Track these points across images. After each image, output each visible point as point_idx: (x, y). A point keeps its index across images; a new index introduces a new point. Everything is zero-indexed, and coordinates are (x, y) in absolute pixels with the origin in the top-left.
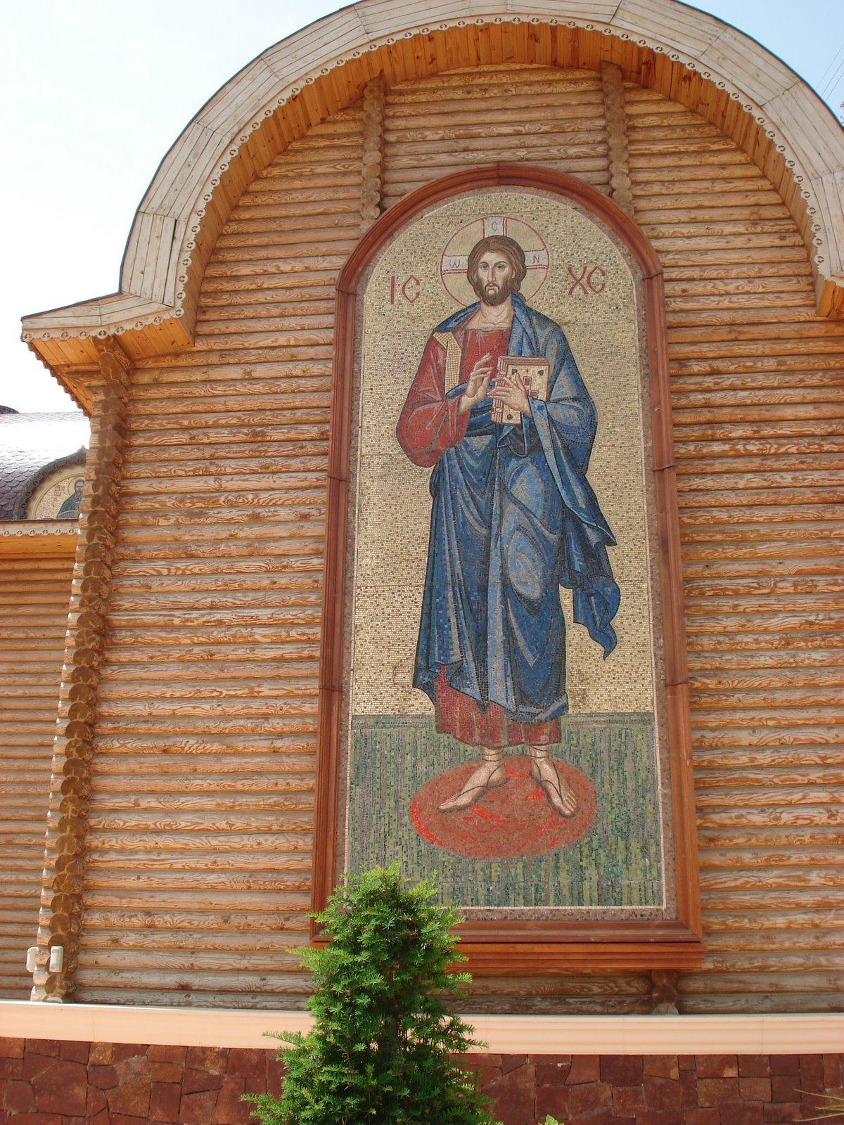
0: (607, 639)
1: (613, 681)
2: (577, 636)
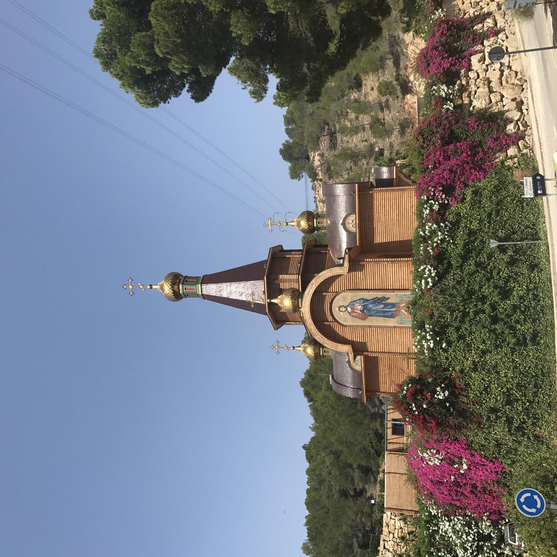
0: (388, 298)
1: (393, 298)
2: (388, 301)
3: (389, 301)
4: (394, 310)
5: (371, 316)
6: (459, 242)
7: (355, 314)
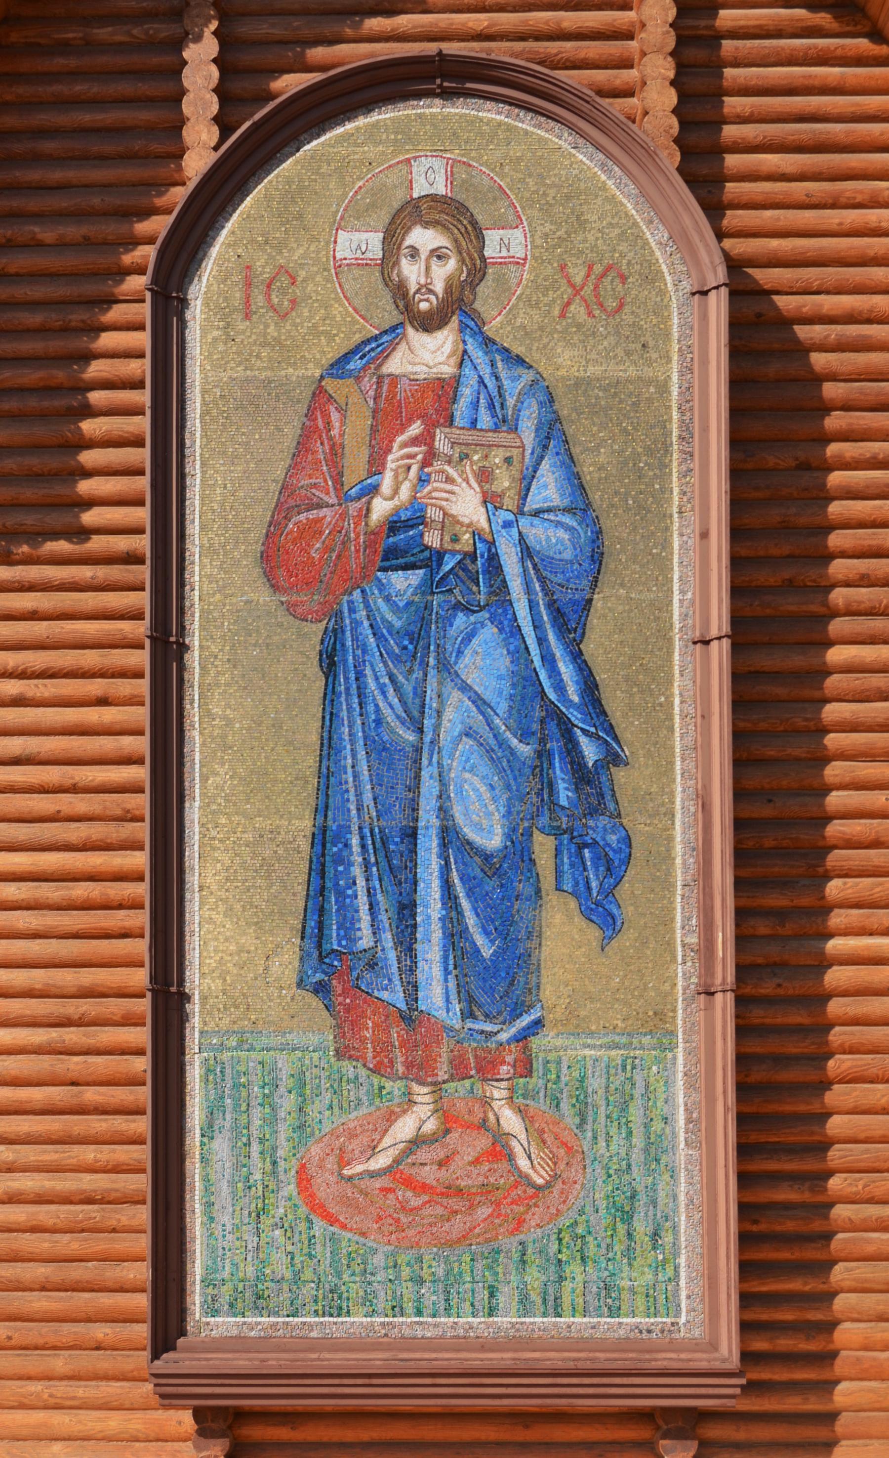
3: (561, 931)
4: (436, 994)
5: (330, 662)
6: (199, 81)
7: (352, 428)
